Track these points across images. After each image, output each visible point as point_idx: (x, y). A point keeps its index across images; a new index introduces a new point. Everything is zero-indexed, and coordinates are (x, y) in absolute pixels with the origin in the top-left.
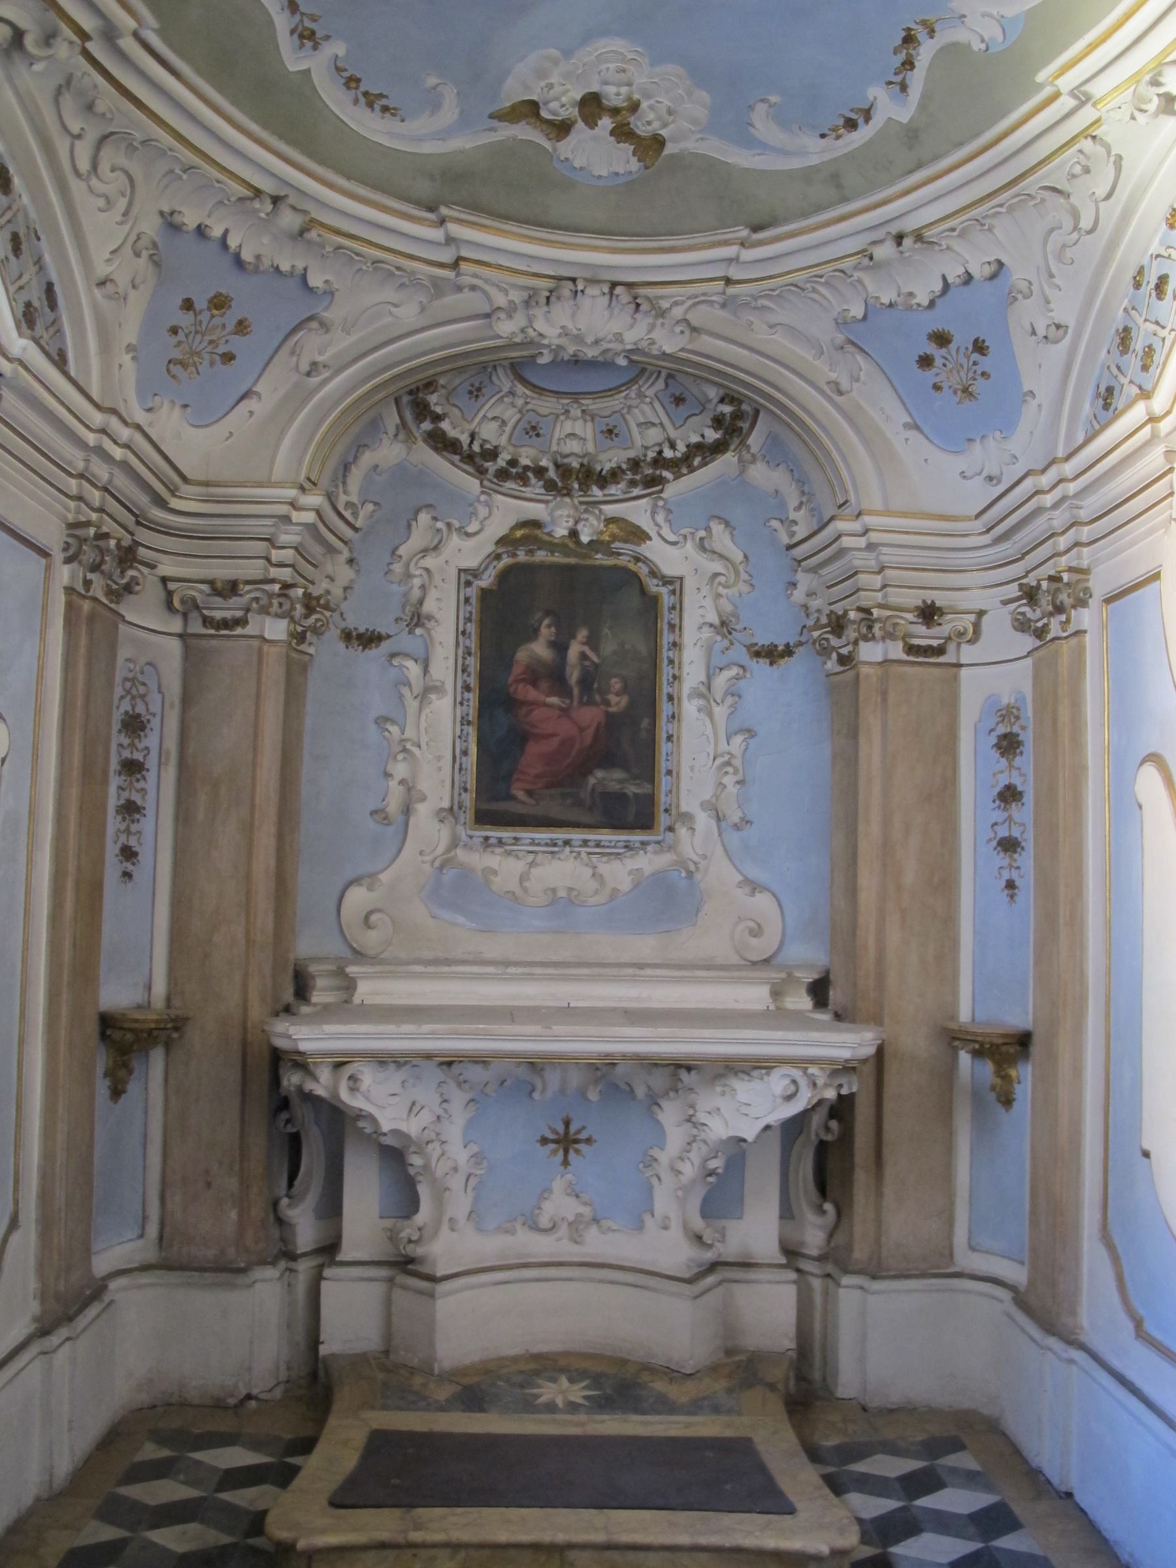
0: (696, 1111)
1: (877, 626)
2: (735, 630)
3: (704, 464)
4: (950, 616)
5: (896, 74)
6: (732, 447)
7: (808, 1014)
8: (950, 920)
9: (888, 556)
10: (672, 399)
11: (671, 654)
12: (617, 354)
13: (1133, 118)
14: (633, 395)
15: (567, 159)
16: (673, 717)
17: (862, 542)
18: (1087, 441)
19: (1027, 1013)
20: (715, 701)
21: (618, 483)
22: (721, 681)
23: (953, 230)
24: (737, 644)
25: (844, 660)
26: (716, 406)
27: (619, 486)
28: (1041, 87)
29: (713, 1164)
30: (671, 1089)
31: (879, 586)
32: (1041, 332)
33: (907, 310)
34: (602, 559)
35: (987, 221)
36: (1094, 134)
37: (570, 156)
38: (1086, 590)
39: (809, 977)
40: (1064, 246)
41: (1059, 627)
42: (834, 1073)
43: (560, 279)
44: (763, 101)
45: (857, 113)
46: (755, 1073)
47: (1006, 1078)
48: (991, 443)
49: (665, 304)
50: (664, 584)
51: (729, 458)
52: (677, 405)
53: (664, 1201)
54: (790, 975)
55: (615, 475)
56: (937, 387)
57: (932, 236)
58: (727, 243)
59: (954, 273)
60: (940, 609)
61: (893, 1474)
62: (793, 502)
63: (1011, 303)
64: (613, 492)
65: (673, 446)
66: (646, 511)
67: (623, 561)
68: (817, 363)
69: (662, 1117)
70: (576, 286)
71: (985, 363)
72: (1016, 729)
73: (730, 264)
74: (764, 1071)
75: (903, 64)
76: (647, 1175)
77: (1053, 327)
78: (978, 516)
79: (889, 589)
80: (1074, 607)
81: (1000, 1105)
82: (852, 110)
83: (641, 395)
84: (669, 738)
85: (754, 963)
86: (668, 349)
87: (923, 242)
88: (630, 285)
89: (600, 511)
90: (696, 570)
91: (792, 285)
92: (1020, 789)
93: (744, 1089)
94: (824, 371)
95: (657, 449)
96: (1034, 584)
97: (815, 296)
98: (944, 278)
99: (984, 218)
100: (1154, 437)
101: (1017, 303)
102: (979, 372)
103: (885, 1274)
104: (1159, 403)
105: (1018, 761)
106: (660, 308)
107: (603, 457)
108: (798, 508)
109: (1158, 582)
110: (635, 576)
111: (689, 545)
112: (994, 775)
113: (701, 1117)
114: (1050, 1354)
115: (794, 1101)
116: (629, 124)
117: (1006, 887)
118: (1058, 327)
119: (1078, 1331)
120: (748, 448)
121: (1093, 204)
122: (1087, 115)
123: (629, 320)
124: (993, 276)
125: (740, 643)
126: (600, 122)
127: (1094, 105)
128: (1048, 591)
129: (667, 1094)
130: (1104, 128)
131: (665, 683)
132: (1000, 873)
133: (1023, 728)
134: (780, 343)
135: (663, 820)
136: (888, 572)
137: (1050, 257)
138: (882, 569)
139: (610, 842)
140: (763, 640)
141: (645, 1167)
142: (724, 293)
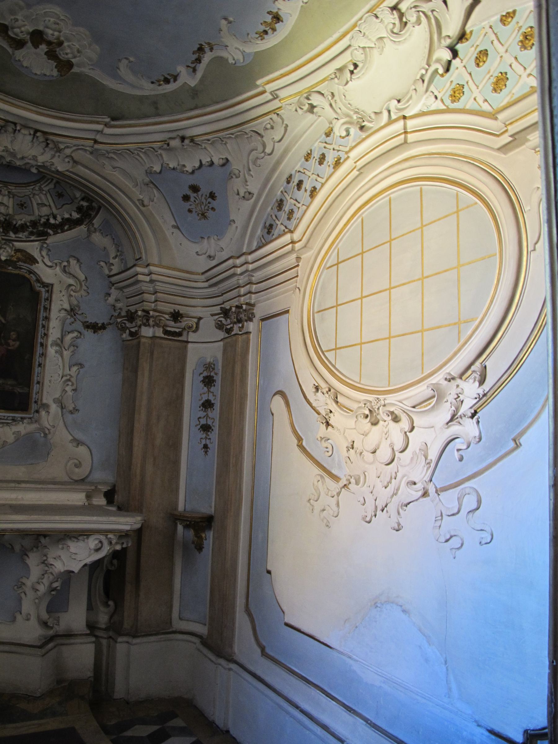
0: (47, 558)
1: (151, 320)
2: (77, 314)
3: (69, 229)
4: (186, 319)
5: (192, 63)
6: (85, 223)
7: (104, 507)
8: (176, 463)
9: (159, 287)
10: (57, 194)
11: (44, 322)
12: (33, 166)
13: (296, 110)
14: (37, 188)
15: (19, 60)
16: (43, 354)
17: (147, 279)
18: (259, 248)
19: (211, 507)
20: (64, 348)
21: (24, 232)
22: (68, 338)
23: (209, 140)
24: (78, 322)
25: (132, 334)
26: (80, 201)
27: (25, 234)
28: (257, 86)
29: (55, 585)
30: (35, 547)
31: (153, 300)
32: (242, 194)
33: (181, 172)
34: (11, 270)
35: (225, 140)
36: (278, 113)
37: (22, 60)
38: (253, 314)
39: (105, 488)
40: (257, 158)
41: (238, 329)
42: (121, 537)
43: (7, 121)
44: (127, 59)
45: (170, 76)
46: (81, 538)
47: (200, 538)
48: (212, 241)
49: (62, 146)
50: (44, 287)
51: (83, 228)
52: (59, 198)
53: (27, 606)
54: (96, 487)
55: (23, 228)
56: (190, 211)
57: (199, 141)
58: (98, 123)
59: (206, 160)
60: (181, 315)
61: (145, 734)
62: (112, 255)
63: (230, 179)
64: (20, 236)
65: (55, 218)
66: (37, 248)
67: (23, 272)
68: (134, 189)
69: (28, 561)
70: (16, 127)
71: (214, 204)
72: (212, 374)
73: (98, 133)
74: (85, 537)
75: (196, 60)
76: (19, 592)
77: (247, 194)
78: (203, 273)
79: (159, 303)
80: (246, 321)
81: (196, 550)
82: (168, 74)
83: (41, 189)
84: (40, 365)
85: (76, 481)
86: (60, 169)
87: (194, 143)
88: (44, 133)
89: (13, 245)
90: (60, 281)
91: (128, 150)
92: (213, 402)
93: (74, 546)
94: (137, 194)
95: (46, 218)
96: (228, 307)
97: (137, 157)
98: (201, 161)
99: (223, 138)
100: (293, 250)
101: (232, 179)
102: (210, 207)
103: (139, 634)
104: (296, 236)
105: (212, 389)
106: (59, 148)
107: (16, 217)
108: (115, 258)
109: (288, 315)
110: (29, 280)
111: (58, 268)
112: (201, 395)
113: (51, 561)
114: (220, 667)
115: (99, 552)
116: (56, 51)
117: (204, 448)
118: (250, 193)
119: (233, 655)
120: (93, 224)
121: (272, 143)
122: (275, 104)
123: (42, 151)
124: (223, 165)
125: (80, 321)
126: (40, 46)
127: (280, 100)
128: (235, 312)
129: (32, 549)
130: (282, 111)
131: (40, 337)
132: (201, 441)
133: (216, 374)
134: (118, 177)
135: (34, 407)
136: (159, 295)
137: (250, 161)
138: (155, 293)
139: (4, 417)
140: (91, 319)
141: (18, 588)
142: (93, 147)
